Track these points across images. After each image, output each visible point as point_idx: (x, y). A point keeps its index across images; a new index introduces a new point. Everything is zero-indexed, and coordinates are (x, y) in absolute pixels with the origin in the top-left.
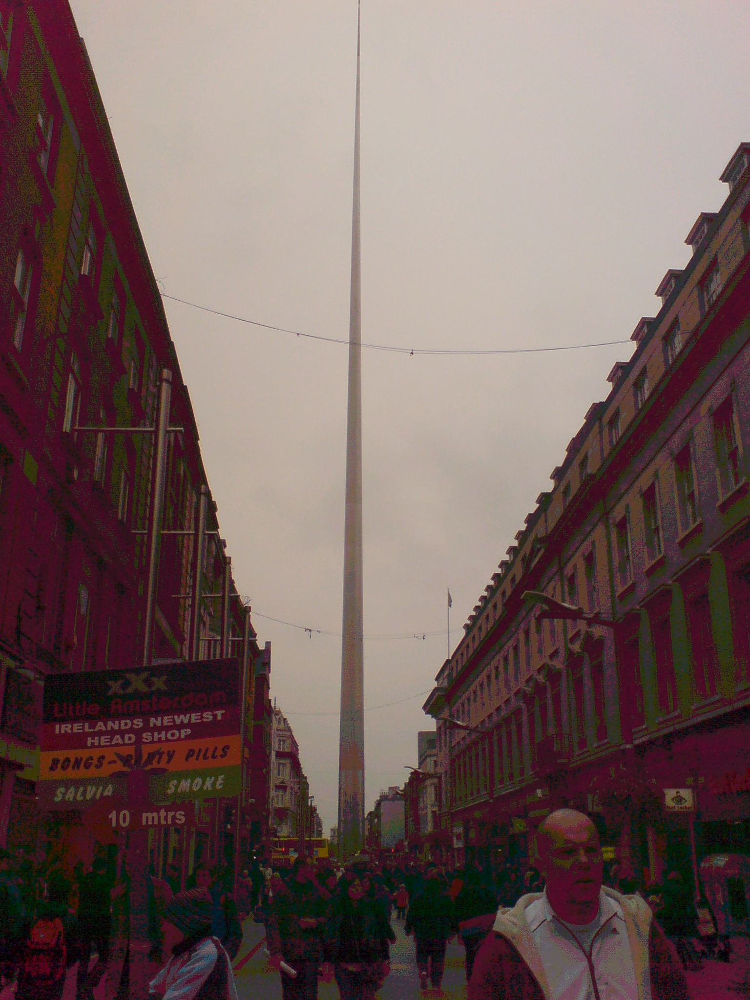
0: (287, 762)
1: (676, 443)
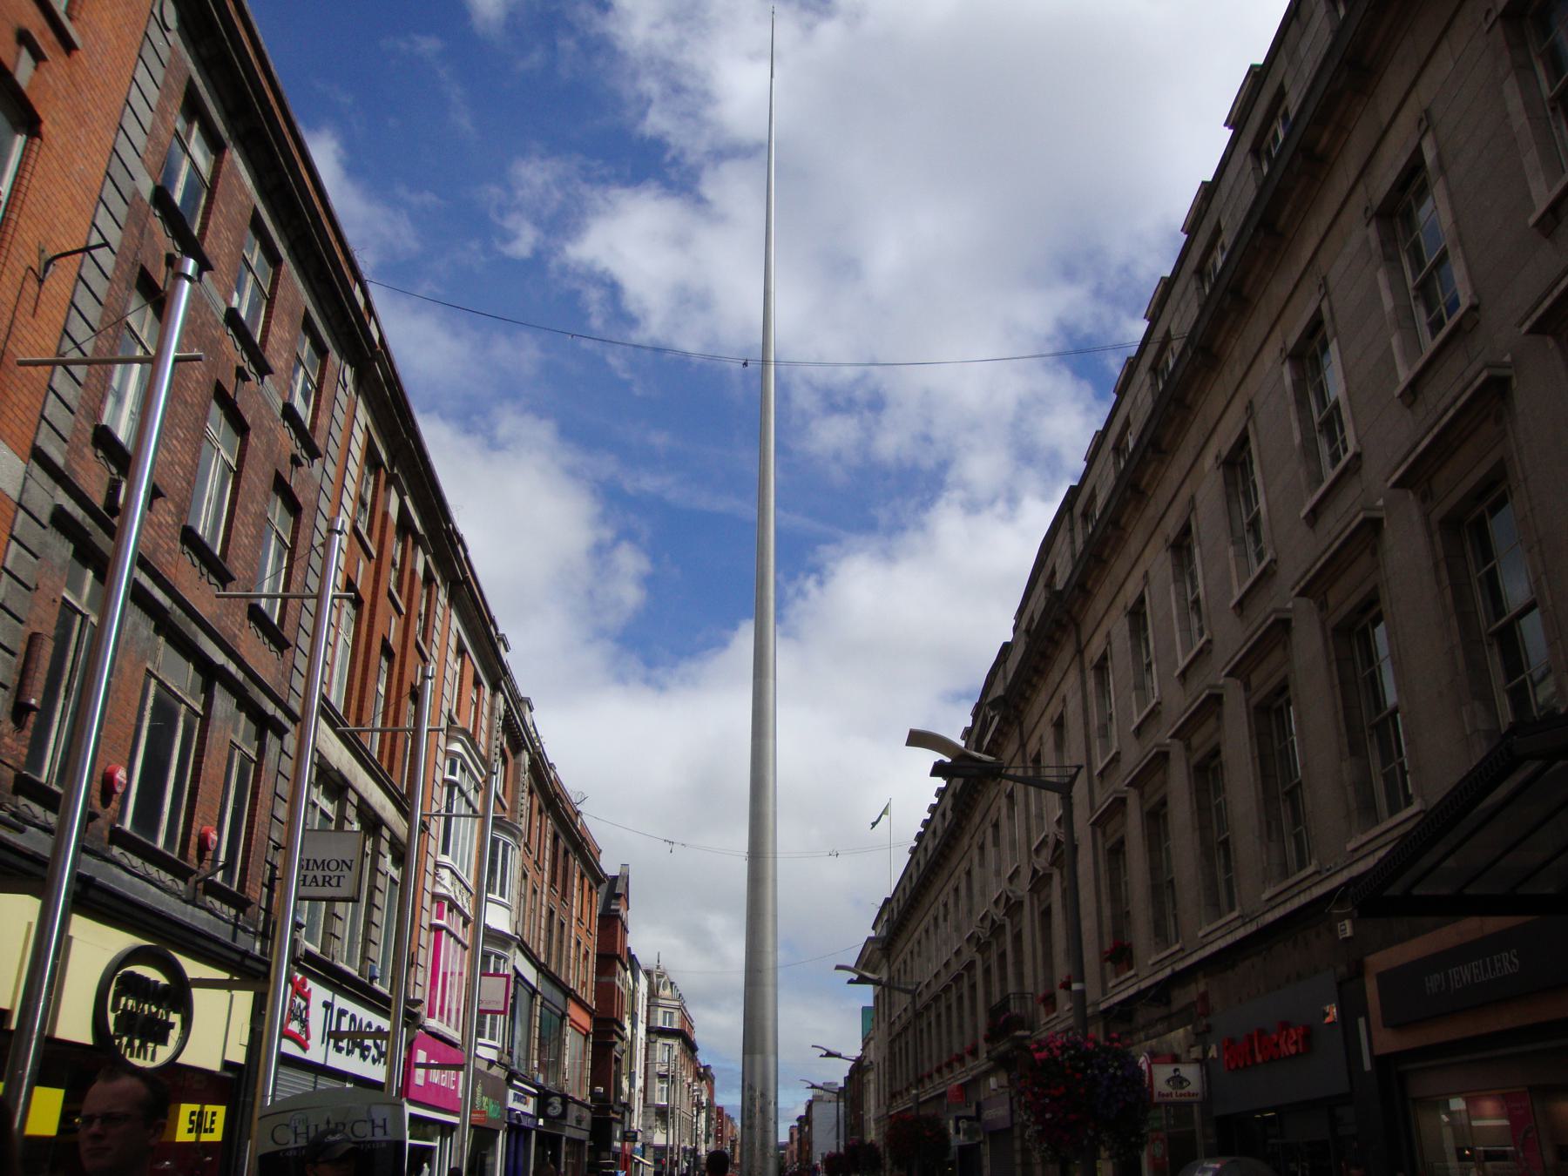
0: (676, 1044)
1: (1171, 526)
